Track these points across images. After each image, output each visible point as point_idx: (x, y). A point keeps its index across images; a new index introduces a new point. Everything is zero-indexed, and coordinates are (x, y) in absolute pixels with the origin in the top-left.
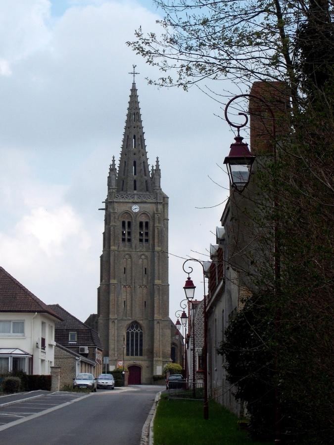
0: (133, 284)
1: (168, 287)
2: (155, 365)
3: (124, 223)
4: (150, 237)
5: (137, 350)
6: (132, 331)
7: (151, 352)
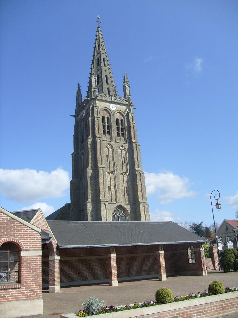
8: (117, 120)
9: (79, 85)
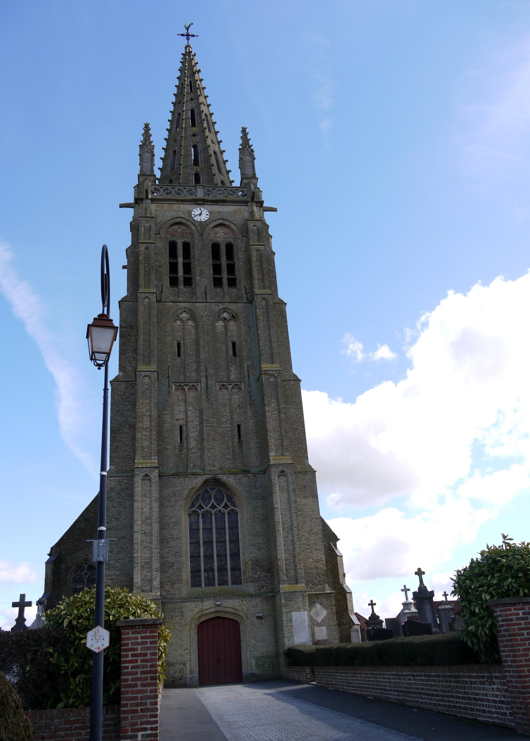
0: (203, 379)
1: (315, 477)
2: (284, 610)
3: (173, 246)
4: (240, 274)
5: (222, 569)
6: (207, 508)
7: (269, 568)
8: (216, 247)
9: (244, 131)
